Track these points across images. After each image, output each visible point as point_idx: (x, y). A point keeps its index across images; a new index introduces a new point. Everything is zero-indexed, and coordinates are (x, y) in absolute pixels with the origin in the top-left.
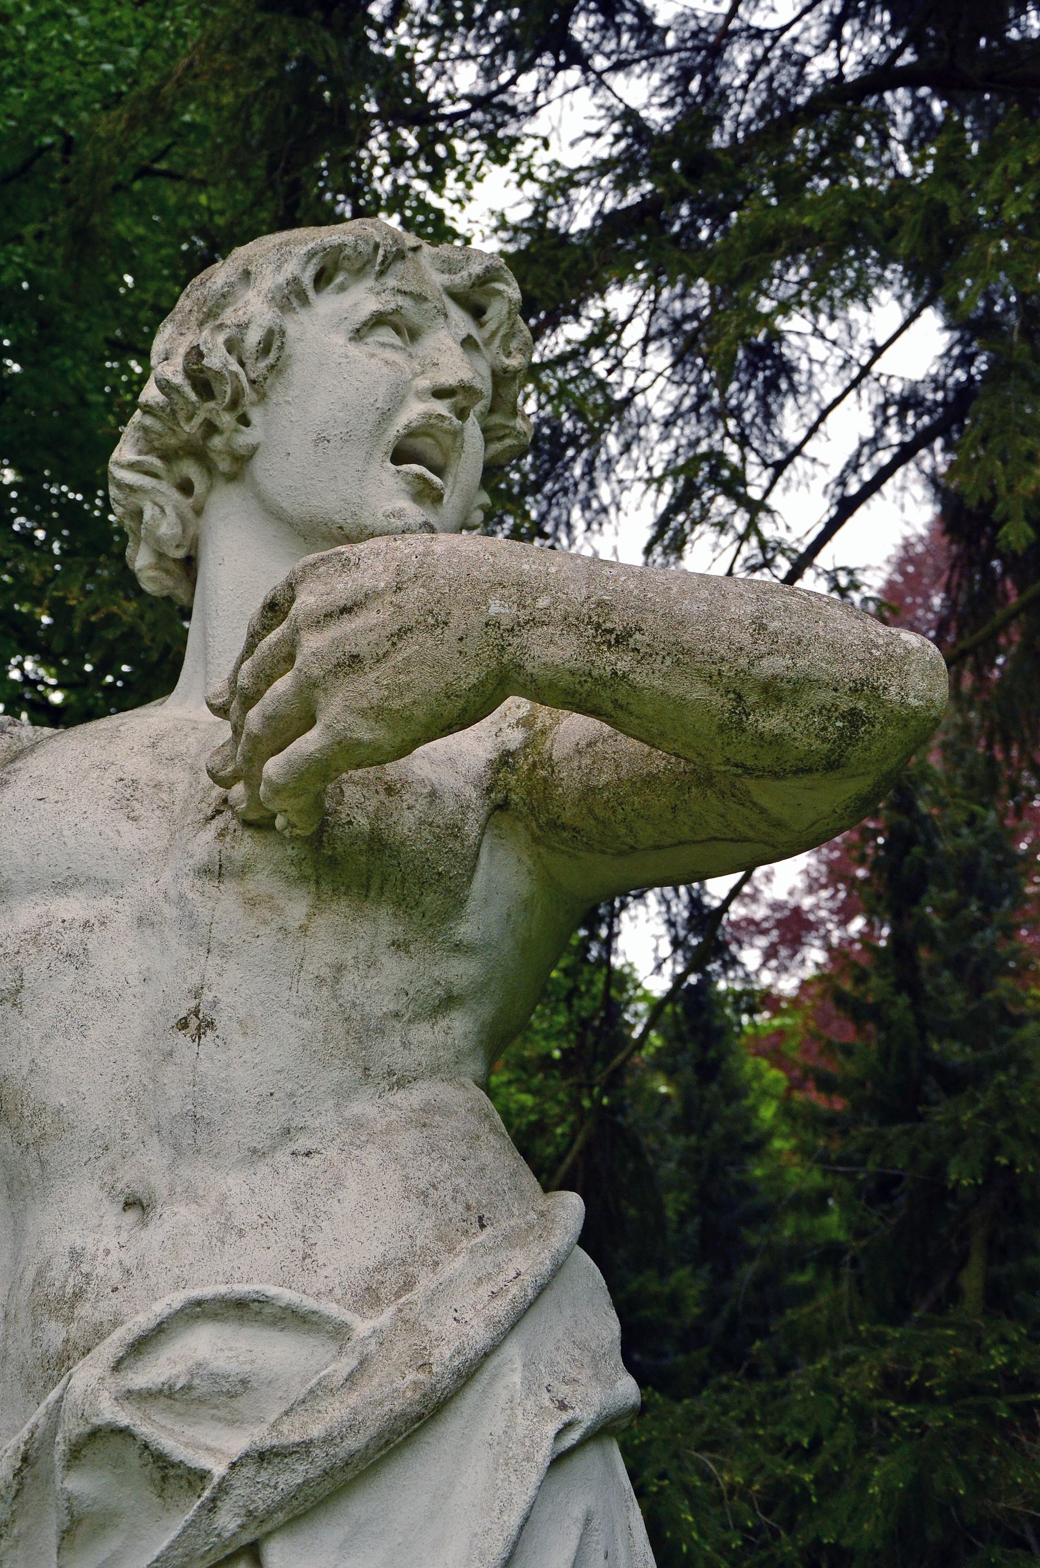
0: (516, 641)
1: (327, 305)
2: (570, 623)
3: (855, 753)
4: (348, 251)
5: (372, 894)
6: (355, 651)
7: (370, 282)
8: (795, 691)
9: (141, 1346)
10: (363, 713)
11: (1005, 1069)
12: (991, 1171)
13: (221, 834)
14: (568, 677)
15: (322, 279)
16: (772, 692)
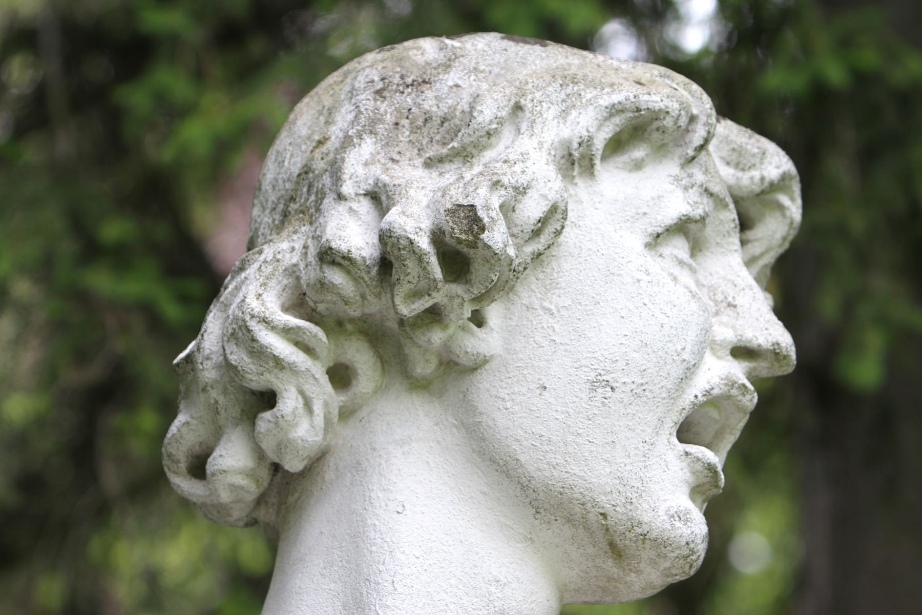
1: (614, 182)
4: (668, 122)
7: (672, 167)
15: (616, 145)
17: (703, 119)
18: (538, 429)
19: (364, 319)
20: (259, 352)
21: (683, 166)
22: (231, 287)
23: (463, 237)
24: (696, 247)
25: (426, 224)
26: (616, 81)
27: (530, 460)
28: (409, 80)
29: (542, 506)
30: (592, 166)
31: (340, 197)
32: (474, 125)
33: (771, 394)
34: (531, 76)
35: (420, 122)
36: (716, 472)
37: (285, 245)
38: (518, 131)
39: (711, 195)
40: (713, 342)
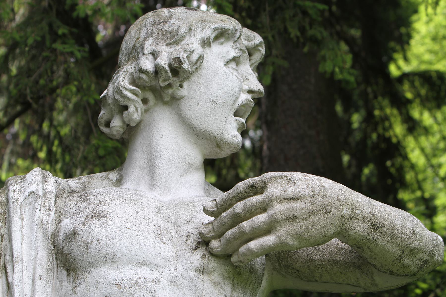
0: (349, 223)
1: (216, 48)
2: (365, 220)
4: (230, 32)
5: (247, 286)
6: (295, 214)
7: (231, 43)
8: (417, 253)
10: (293, 235)
14: (360, 237)
15: (216, 38)
16: (413, 252)
17: (239, 30)
18: (197, 115)
19: (151, 86)
20: (123, 96)
21: (234, 43)
22: (115, 78)
23: (177, 66)
24: (238, 64)
25: (167, 62)
26: (216, 21)
27: (195, 123)
28: (161, 21)
29: (198, 135)
30: (210, 44)
31: (144, 54)
32: (179, 35)
33: (258, 101)
34: (193, 20)
35: (164, 33)
36: (244, 124)
37: (129, 67)
38: (190, 35)
39: (242, 50)
40: (243, 89)
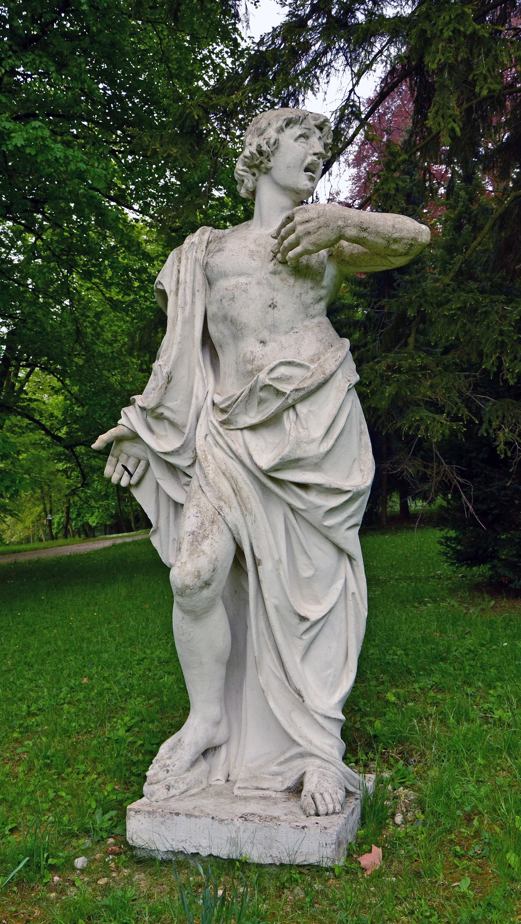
2: (355, 226)
3: (411, 252)
7: (298, 126)
9: (272, 370)
11: (417, 264)
12: (419, 312)
13: (275, 264)
15: (287, 125)
16: (395, 241)
